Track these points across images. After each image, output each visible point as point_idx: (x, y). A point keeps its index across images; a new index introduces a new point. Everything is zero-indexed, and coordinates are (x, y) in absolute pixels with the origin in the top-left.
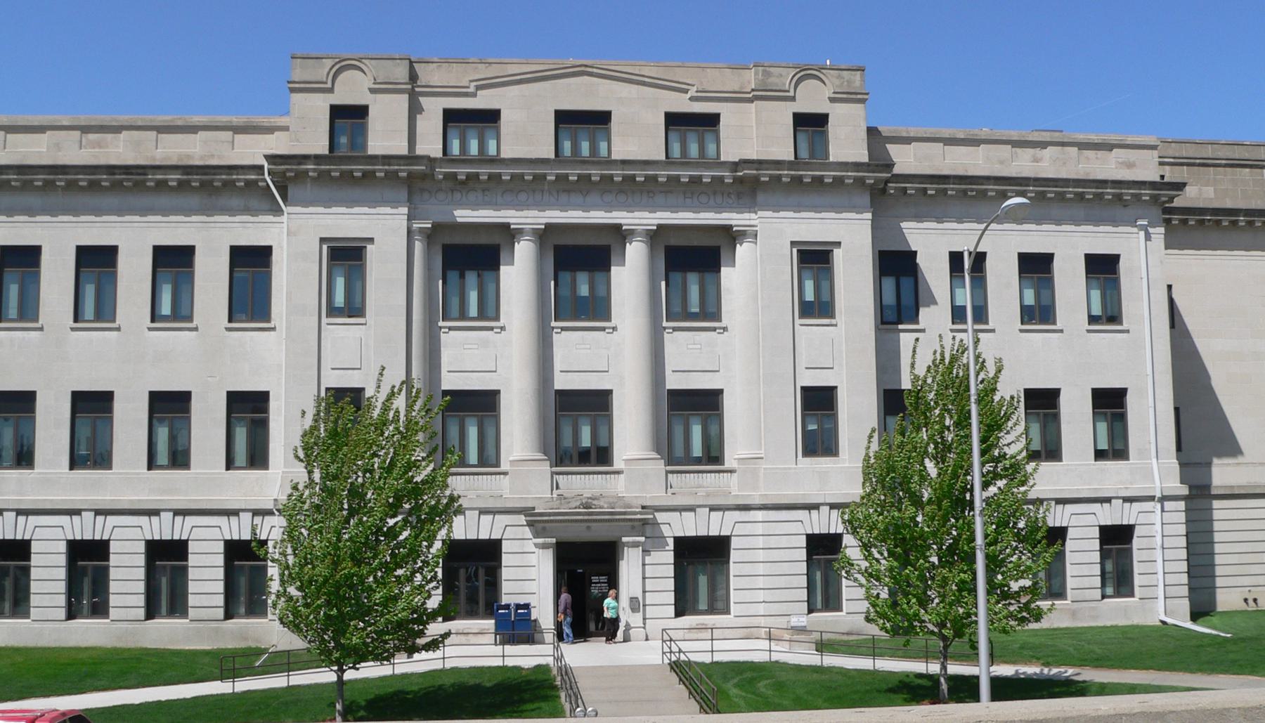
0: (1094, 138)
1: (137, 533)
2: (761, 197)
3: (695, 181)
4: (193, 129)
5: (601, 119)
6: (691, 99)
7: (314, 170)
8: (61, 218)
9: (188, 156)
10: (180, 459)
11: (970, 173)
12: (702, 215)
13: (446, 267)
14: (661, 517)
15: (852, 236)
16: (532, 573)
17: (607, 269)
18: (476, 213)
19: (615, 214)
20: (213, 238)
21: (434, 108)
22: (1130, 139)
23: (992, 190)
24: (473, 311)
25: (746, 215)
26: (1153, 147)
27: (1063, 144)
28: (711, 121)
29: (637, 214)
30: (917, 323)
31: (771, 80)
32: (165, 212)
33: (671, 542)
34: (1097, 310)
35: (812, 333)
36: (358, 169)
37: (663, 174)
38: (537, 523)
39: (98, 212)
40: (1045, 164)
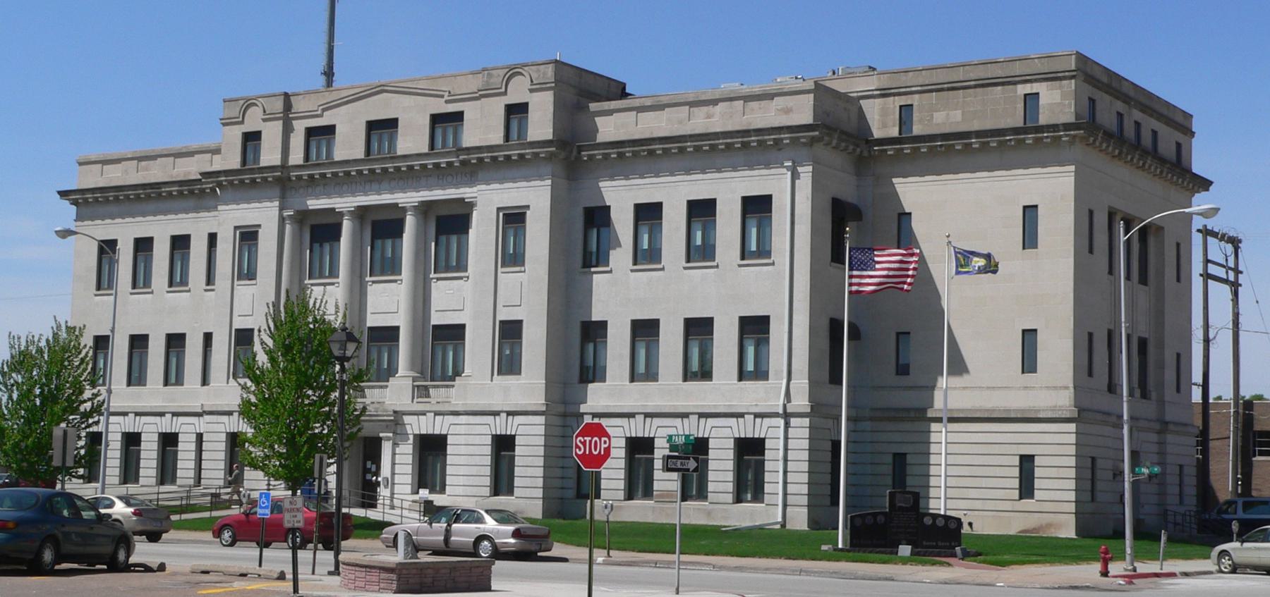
0: (757, 89)
1: (727, 432)
2: (480, 175)
3: (521, 156)
5: (392, 124)
6: (447, 102)
10: (705, 373)
12: (448, 191)
13: (374, 237)
14: (407, 419)
21: (300, 127)
27: (731, 99)
28: (458, 117)
29: (409, 194)
33: (411, 437)
37: (365, 168)
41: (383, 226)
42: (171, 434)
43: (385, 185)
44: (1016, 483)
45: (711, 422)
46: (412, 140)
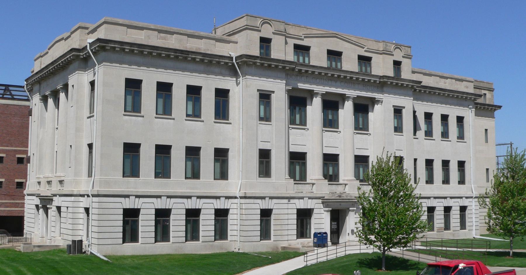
0: (460, 77)
1: (182, 206)
3: (397, 84)
4: (201, 37)
6: (365, 51)
7: (259, 63)
8: (151, 69)
9: (199, 49)
11: (458, 90)
15: (279, 89)
16: (323, 221)
17: (337, 109)
18: (304, 85)
19: (312, 86)
20: (209, 84)
23: (164, 54)
24: (298, 121)
25: (380, 95)
26: (472, 82)
27: (452, 78)
28: (369, 59)
29: (351, 91)
30: (448, 138)
31: (387, 47)
32: (192, 71)
34: (190, 112)
35: (264, 127)
36: (266, 63)
37: (355, 77)
38: (326, 203)
39: (166, 68)
40: (447, 84)
41: (331, 105)
42: (224, 209)
43: (338, 83)
45: (142, 200)
46: (349, 64)
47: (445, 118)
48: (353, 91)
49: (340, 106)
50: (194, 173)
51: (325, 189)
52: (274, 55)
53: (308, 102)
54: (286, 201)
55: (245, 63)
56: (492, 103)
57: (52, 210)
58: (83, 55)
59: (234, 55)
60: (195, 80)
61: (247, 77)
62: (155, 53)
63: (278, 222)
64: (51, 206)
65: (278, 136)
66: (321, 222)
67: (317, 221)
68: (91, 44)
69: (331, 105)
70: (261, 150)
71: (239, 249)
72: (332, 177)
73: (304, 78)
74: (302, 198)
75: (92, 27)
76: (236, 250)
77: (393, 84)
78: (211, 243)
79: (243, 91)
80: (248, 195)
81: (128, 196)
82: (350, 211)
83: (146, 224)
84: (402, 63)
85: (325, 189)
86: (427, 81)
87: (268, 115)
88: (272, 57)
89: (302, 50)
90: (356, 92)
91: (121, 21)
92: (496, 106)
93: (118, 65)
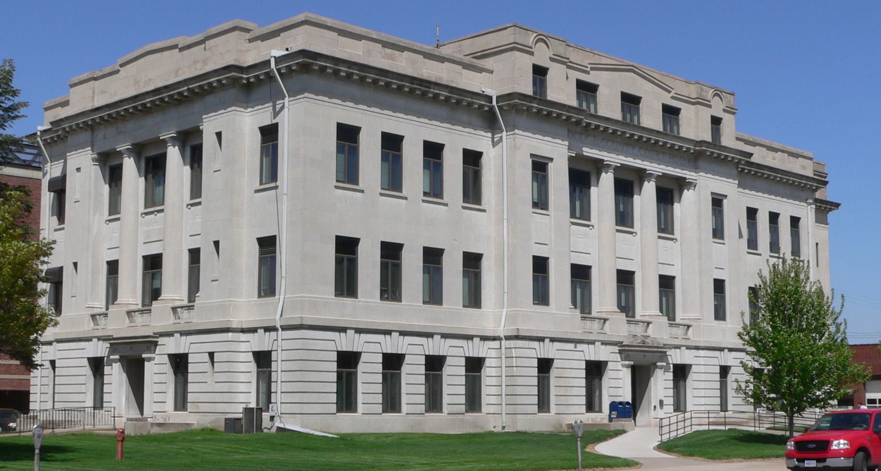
2: (701, 163)
6: (673, 98)
8: (373, 109)
16: (620, 383)
20: (457, 140)
22: (214, 30)
24: (578, 215)
27: (783, 151)
29: (653, 165)
33: (672, 366)
38: (625, 351)
41: (626, 186)
44: (535, 400)
47: (774, 217)
48: (656, 165)
49: (636, 190)
50: (434, 294)
51: (620, 328)
52: (551, 96)
53: (593, 180)
54: (571, 346)
55: (514, 106)
56: (824, 199)
57: (156, 361)
58: (248, 79)
59: (493, 93)
60: (437, 132)
61: (516, 131)
62: (382, 81)
63: (562, 382)
64: (153, 355)
65: (559, 237)
66: (618, 384)
67: (613, 383)
68: (278, 60)
69: (626, 186)
70: (535, 258)
71: (504, 428)
72: (627, 307)
73: (590, 139)
74: (592, 342)
75: (258, 31)
76: (498, 429)
77: (708, 155)
78: (460, 417)
79: (507, 156)
80: (522, 334)
81: (343, 330)
82: (657, 367)
83: (369, 379)
84: (723, 121)
85: (620, 328)
86: (760, 156)
87: (543, 198)
88: (549, 98)
89: (587, 89)
90: (661, 166)
91: (329, 22)
92: (831, 203)
93: (326, 99)
